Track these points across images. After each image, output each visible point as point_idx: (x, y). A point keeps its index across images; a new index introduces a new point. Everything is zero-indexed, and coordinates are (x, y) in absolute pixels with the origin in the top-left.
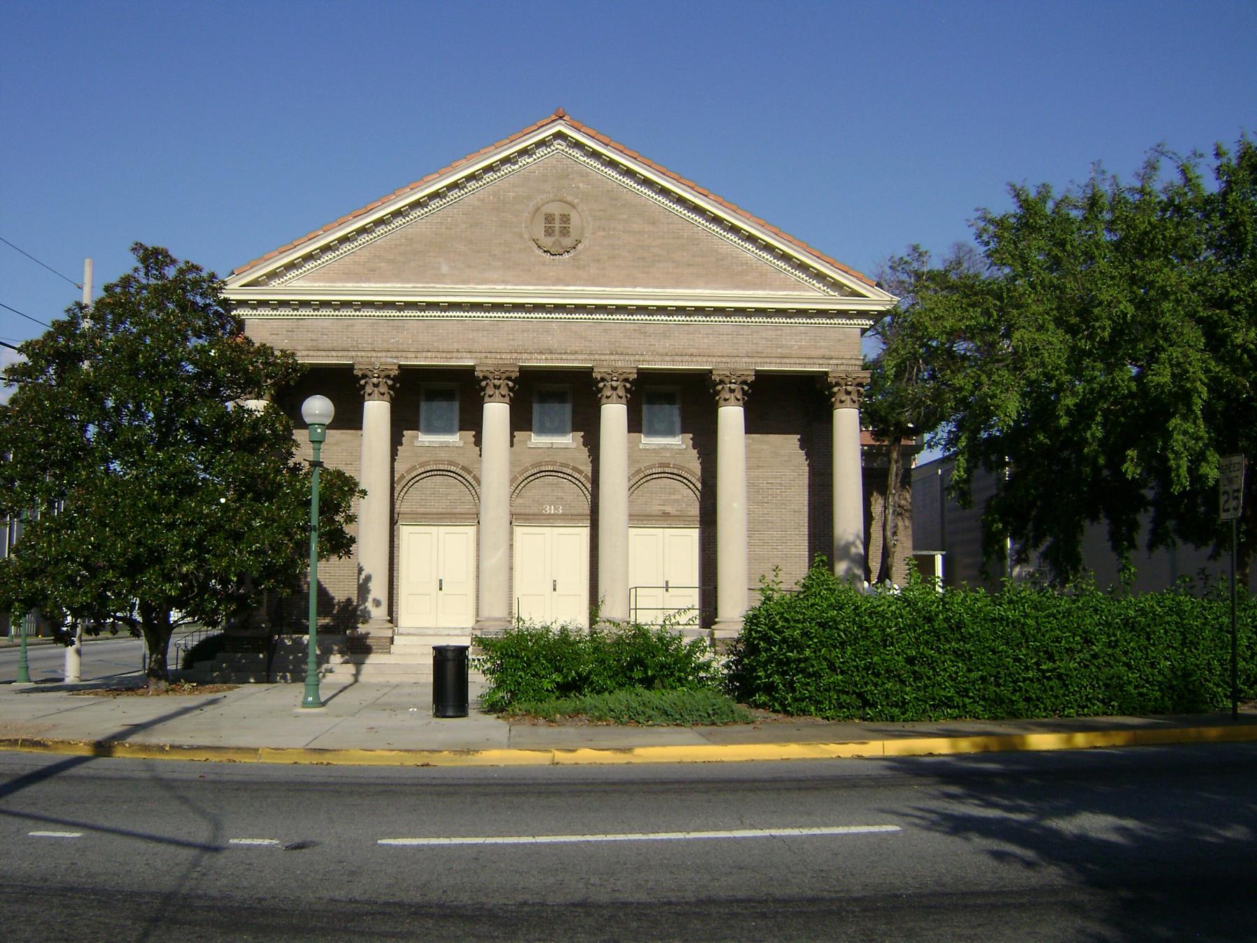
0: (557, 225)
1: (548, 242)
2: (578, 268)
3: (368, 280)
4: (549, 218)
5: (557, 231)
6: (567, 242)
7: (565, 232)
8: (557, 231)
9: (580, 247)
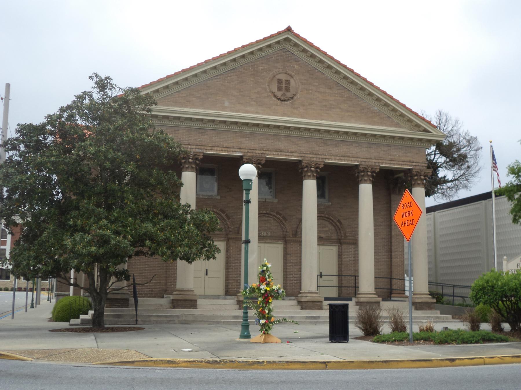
0: (284, 85)
1: (279, 94)
2: (294, 108)
3: (186, 106)
4: (280, 81)
5: (284, 88)
6: (289, 95)
7: (288, 89)
8: (284, 88)
9: (295, 98)
